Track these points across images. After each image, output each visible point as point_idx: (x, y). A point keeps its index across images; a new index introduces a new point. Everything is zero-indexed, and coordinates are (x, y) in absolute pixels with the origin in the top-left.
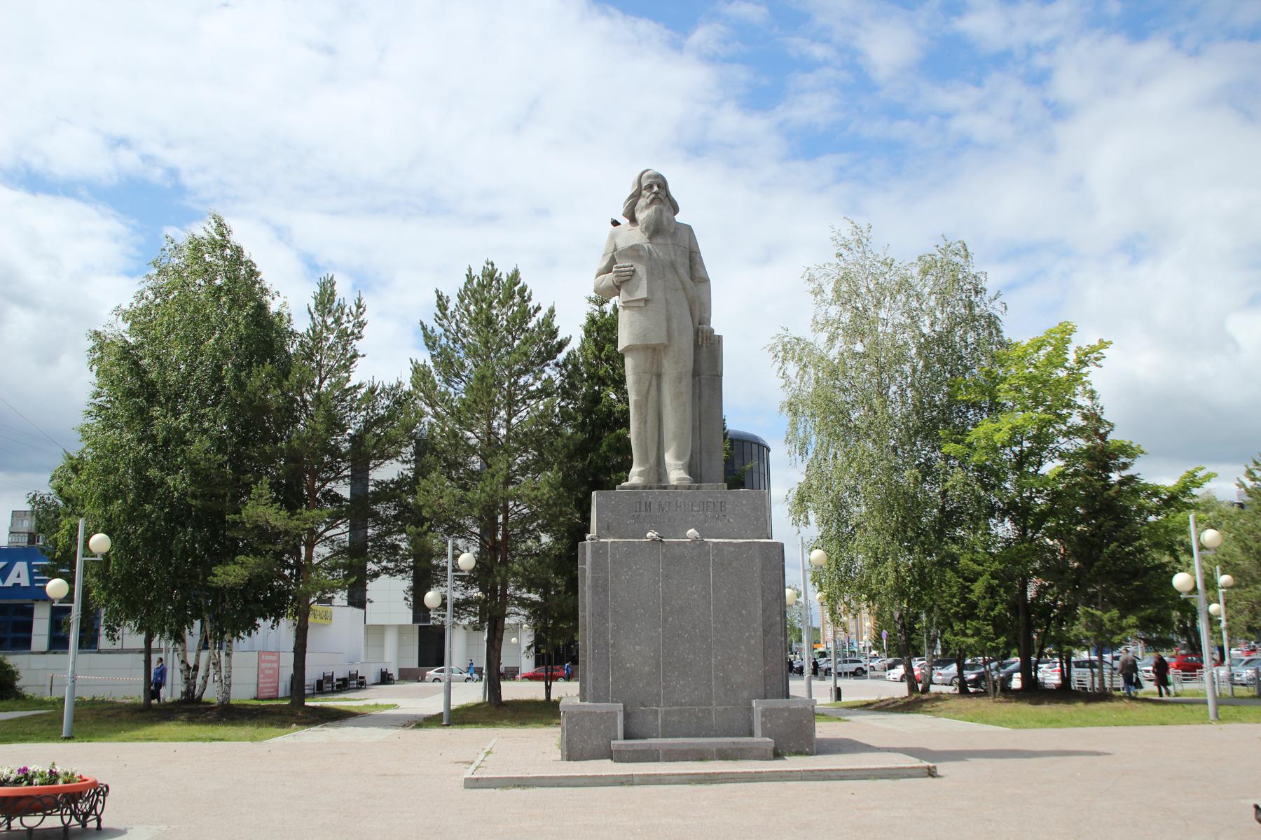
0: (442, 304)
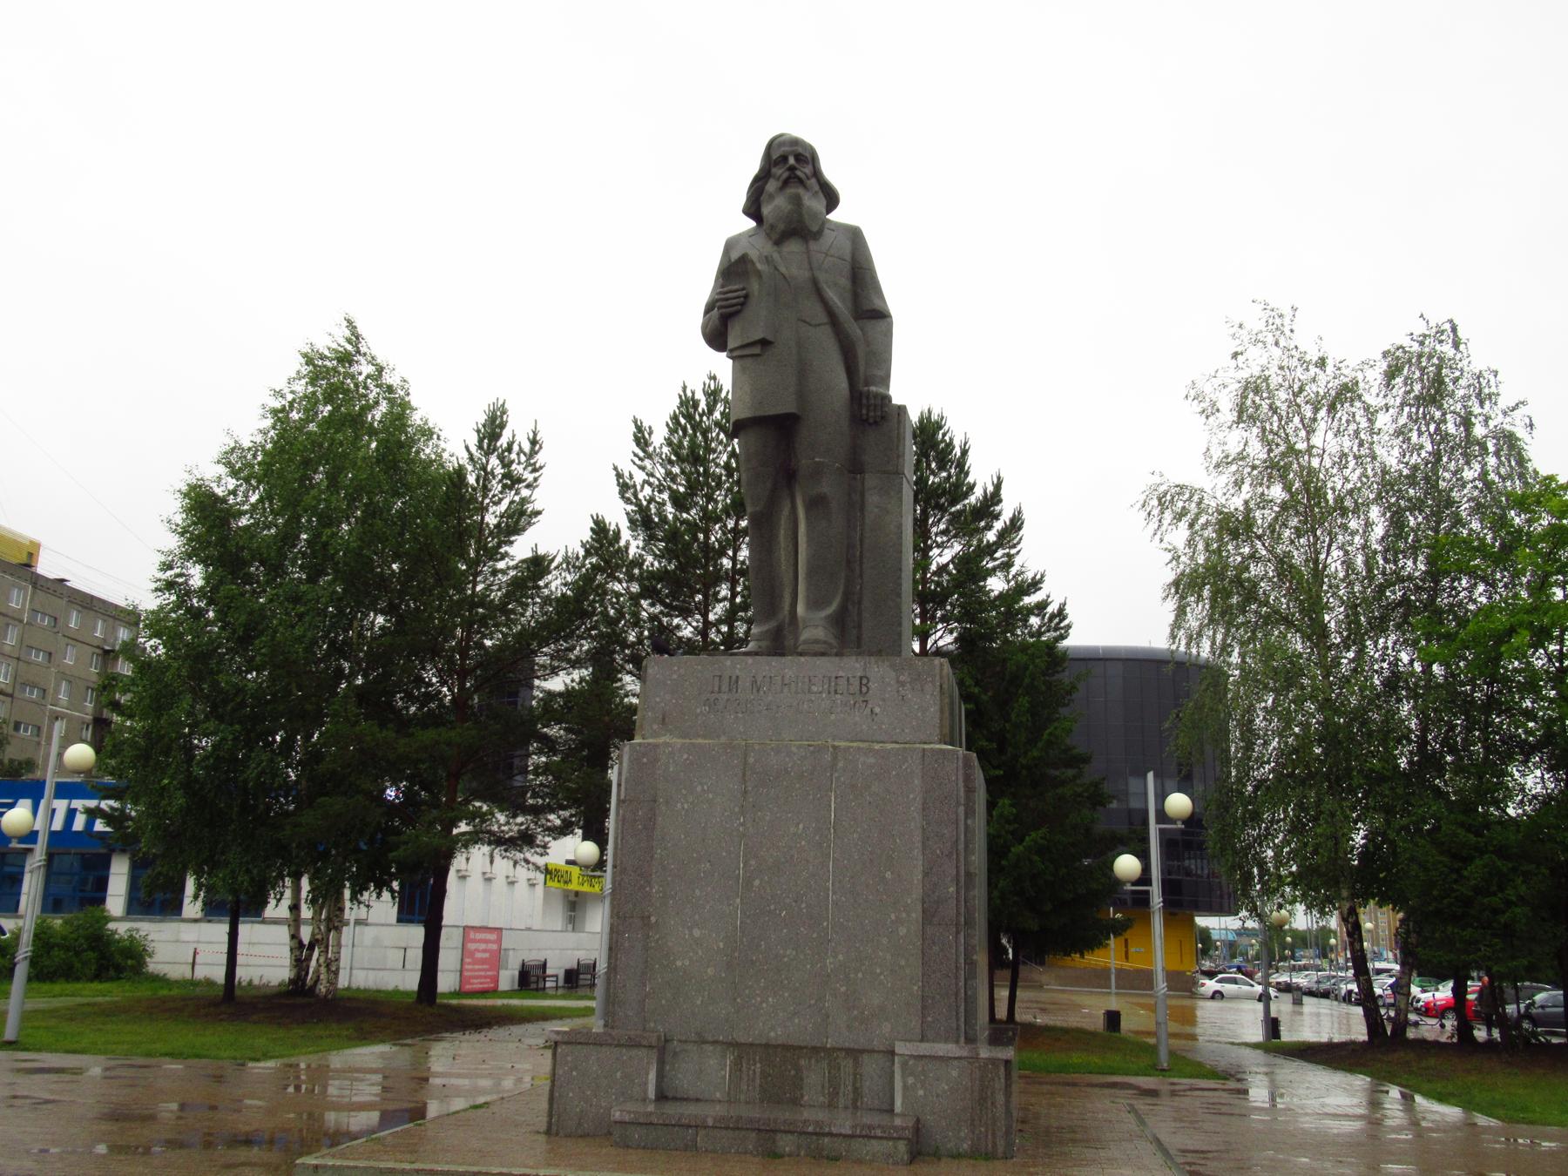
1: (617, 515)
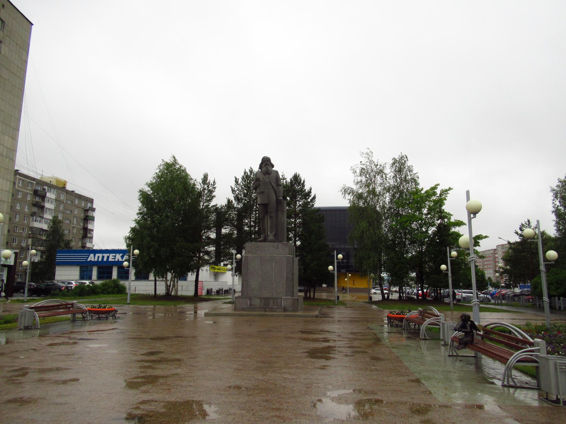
0: (236, 181)
1: (232, 198)
